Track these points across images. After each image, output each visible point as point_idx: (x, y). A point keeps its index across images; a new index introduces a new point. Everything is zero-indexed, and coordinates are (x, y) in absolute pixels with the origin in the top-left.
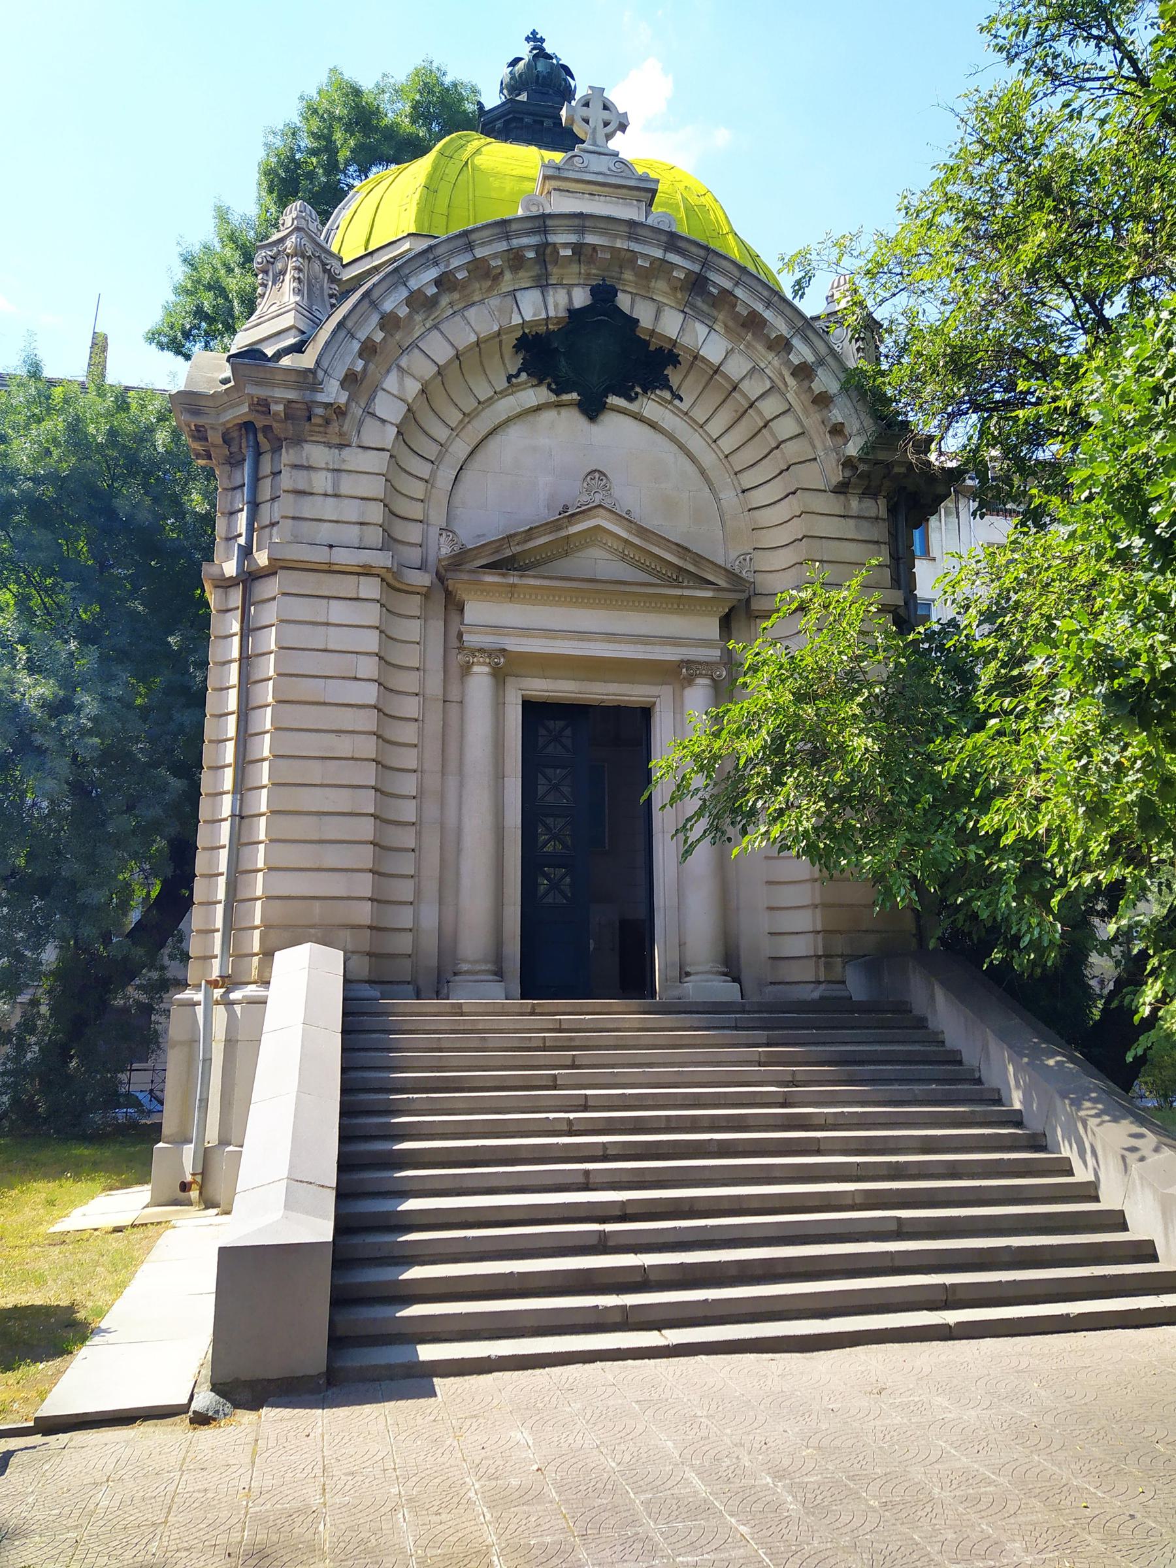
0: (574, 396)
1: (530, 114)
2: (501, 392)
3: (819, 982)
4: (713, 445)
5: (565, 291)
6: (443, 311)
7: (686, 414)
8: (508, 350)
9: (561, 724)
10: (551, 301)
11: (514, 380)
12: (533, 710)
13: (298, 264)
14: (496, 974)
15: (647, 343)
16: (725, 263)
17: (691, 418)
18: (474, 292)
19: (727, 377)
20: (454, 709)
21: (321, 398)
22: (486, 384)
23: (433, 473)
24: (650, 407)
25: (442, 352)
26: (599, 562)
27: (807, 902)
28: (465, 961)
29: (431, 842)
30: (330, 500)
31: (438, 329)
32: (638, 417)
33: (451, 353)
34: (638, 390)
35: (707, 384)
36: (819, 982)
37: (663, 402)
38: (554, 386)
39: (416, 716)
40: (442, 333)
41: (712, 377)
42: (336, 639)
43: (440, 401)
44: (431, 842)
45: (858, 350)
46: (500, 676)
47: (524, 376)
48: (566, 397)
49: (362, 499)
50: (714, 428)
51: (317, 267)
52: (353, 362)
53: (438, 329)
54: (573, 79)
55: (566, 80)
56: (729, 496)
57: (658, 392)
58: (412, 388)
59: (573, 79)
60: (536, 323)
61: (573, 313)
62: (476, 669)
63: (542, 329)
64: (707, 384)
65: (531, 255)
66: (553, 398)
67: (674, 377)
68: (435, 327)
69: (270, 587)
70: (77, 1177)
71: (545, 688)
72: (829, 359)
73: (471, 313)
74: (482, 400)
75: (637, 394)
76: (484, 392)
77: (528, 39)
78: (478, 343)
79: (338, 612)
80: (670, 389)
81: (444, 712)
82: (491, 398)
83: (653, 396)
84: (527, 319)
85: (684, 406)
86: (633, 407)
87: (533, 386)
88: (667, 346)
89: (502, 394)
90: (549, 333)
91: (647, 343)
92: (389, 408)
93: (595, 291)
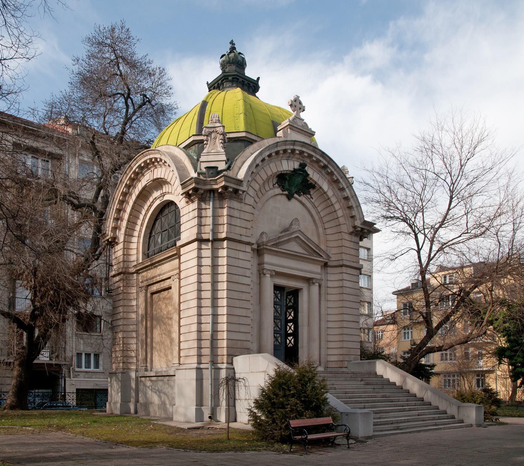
8: (275, 176)
16: (333, 164)
21: (241, 188)
24: (303, 198)
26: (295, 247)
27: (219, 275)
30: (238, 219)
32: (301, 202)
37: (307, 198)
47: (277, 185)
48: (285, 193)
56: (321, 230)
61: (295, 170)
66: (281, 192)
67: (312, 191)
79: (241, 255)
80: (310, 195)
88: (314, 183)
91: (308, 181)
93: (301, 165)
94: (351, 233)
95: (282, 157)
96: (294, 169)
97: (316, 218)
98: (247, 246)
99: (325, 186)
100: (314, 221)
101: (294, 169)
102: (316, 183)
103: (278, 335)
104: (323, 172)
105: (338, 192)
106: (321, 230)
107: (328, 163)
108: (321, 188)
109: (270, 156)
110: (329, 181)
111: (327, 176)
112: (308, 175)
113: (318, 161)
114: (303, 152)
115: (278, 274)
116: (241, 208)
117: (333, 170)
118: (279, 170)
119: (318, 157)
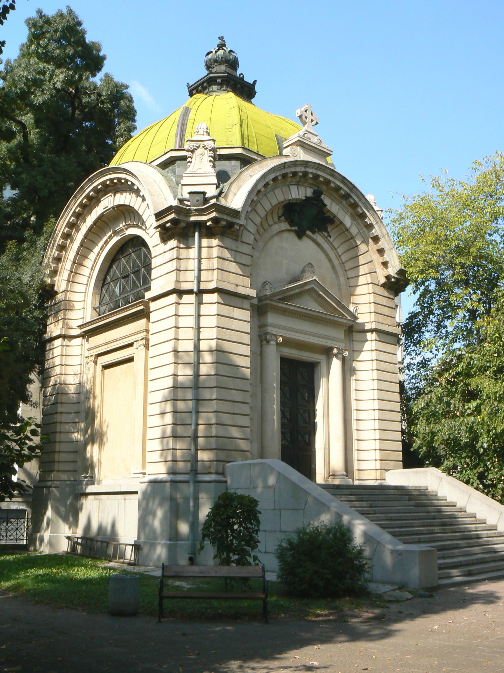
3: (377, 480)
8: (282, 206)
10: (300, 192)
11: (281, 219)
15: (325, 214)
19: (350, 233)
21: (237, 221)
24: (318, 237)
34: (316, 230)
35: (341, 234)
47: (283, 218)
48: (293, 228)
56: (342, 279)
60: (294, 199)
64: (341, 234)
65: (301, 174)
69: (206, 298)
70: (296, 649)
72: (386, 236)
77: (219, 38)
80: (328, 232)
84: (293, 198)
85: (331, 240)
88: (332, 217)
89: (275, 223)
90: (296, 204)
91: (325, 214)
93: (315, 192)
94: (383, 286)
97: (336, 263)
98: (245, 301)
99: (347, 221)
100: (333, 267)
101: (306, 197)
102: (335, 216)
104: (344, 203)
105: (365, 229)
106: (342, 279)
108: (341, 223)
111: (349, 208)
113: (337, 189)
115: (288, 343)
117: (357, 200)
119: (338, 183)
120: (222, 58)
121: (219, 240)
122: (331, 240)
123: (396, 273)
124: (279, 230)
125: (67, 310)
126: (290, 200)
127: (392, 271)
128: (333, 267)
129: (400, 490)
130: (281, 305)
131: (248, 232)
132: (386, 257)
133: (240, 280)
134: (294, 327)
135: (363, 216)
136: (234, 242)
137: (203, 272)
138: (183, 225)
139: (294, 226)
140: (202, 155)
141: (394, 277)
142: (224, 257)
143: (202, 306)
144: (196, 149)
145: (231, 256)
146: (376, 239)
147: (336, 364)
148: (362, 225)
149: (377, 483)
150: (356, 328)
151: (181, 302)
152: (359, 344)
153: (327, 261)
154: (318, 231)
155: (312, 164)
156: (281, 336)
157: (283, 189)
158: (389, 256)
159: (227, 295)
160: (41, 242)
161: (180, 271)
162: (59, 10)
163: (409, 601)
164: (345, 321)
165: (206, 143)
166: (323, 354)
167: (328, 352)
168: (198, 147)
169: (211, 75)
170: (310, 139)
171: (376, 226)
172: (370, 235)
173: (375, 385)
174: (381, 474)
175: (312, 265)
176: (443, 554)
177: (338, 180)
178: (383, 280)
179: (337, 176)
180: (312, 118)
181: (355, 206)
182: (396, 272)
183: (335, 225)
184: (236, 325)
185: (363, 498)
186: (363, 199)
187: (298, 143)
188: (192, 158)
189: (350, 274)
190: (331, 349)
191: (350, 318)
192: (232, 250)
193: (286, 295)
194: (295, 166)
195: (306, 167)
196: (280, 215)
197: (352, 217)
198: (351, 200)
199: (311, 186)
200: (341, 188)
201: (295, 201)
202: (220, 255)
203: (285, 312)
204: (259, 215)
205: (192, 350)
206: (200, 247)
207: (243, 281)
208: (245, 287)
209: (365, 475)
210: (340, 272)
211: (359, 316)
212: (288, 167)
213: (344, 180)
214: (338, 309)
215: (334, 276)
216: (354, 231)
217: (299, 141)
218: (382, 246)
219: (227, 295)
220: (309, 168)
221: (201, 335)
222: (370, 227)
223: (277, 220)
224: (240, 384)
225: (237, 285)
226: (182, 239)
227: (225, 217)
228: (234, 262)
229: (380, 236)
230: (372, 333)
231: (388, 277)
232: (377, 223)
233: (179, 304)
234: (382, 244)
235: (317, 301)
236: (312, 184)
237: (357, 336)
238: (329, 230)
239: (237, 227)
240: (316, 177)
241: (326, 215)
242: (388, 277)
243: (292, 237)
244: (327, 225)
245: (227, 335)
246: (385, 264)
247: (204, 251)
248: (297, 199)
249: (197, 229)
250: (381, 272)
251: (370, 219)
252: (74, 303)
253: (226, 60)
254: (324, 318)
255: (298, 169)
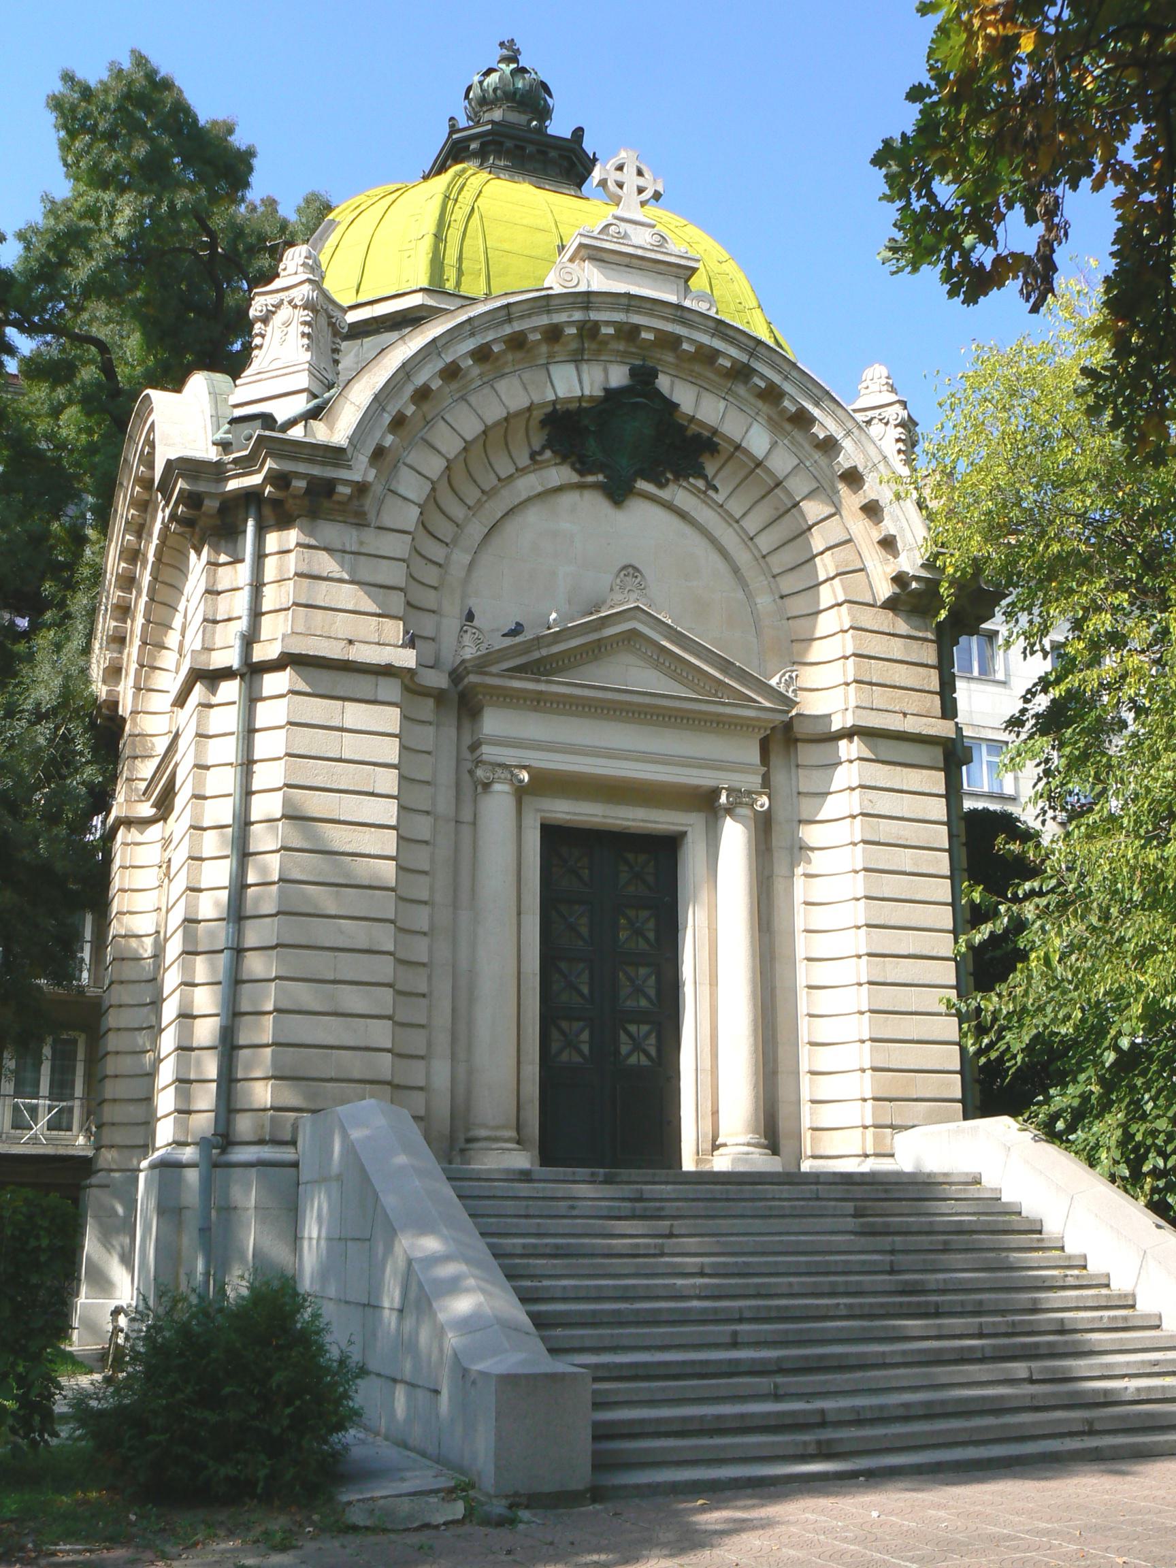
0: (601, 478)
1: (512, 138)
2: (523, 469)
3: (867, 1156)
4: (749, 543)
5: (601, 368)
6: (472, 380)
7: (721, 506)
8: (534, 423)
9: (642, 858)
10: (585, 377)
11: (539, 458)
12: (553, 835)
13: (308, 319)
14: (518, 1143)
17: (727, 512)
18: (506, 363)
19: (768, 471)
20: (466, 831)
21: (343, 474)
22: (506, 459)
23: (447, 557)
24: (679, 495)
25: (471, 428)
28: (485, 1126)
29: (443, 988)
31: (466, 401)
32: (669, 506)
33: (479, 428)
34: (670, 476)
35: (746, 478)
36: (867, 1156)
37: (696, 492)
38: (578, 466)
39: (426, 838)
40: (470, 405)
41: (753, 471)
42: (351, 746)
43: (459, 477)
44: (443, 988)
45: (899, 451)
46: (521, 792)
47: (548, 454)
48: (590, 479)
49: (381, 586)
50: (752, 524)
51: (323, 321)
52: (383, 437)
53: (466, 401)
54: (551, 96)
55: (545, 100)
56: (764, 601)
57: (691, 480)
58: (434, 467)
59: (551, 96)
60: (569, 400)
61: (611, 394)
62: (497, 787)
63: (574, 406)
64: (746, 478)
65: (573, 331)
66: (575, 478)
68: (463, 398)
69: (274, 682)
71: (566, 810)
73: (502, 386)
74: (503, 476)
75: (668, 480)
76: (505, 469)
77: (502, 44)
78: (506, 419)
79: (355, 715)
80: (705, 477)
81: (457, 833)
82: (511, 476)
83: (684, 484)
84: (561, 395)
85: (719, 498)
86: (664, 494)
87: (556, 464)
88: (706, 434)
89: (522, 471)
90: (580, 410)
92: (412, 486)
93: (634, 372)
94: (891, 604)
95: (551, 356)
96: (606, 390)
97: (743, 558)
98: (383, 681)
99: (758, 440)
100: (736, 570)
101: (606, 390)
102: (715, 432)
103: (645, 1028)
104: (741, 390)
105: (817, 455)
106: (764, 601)
107: (751, 355)
108: (738, 447)
109: (482, 355)
110: (770, 419)
111: (760, 404)
112: (676, 406)
113: (708, 356)
114: (637, 329)
115: (546, 784)
116: (361, 543)
117: (777, 379)
118: (537, 399)
119: (705, 339)
120: (495, 90)
121: (301, 529)
122: (719, 498)
123: (923, 566)
124: (540, 489)
125: (136, 758)
126: (554, 403)
127: (910, 562)
128: (736, 570)
129: (882, 1184)
130: (516, 684)
131: (400, 502)
132: (889, 526)
133: (368, 627)
134: (597, 744)
135: (803, 420)
136: (354, 532)
137: (265, 620)
138: (211, 505)
139: (591, 473)
140: (287, 324)
141: (917, 578)
142: (315, 573)
143: (260, 706)
144: (274, 313)
145: (342, 566)
146: (853, 478)
147: (734, 837)
148: (807, 446)
149: (867, 1166)
150: (800, 729)
151: (214, 700)
152: (816, 774)
153: (715, 557)
154: (677, 479)
155: (609, 300)
156: (524, 767)
157: (526, 376)
158: (896, 520)
159: (319, 670)
160: (79, 602)
161: (215, 622)
162: (112, 63)
163: (432, 1532)
164: (751, 713)
165: (293, 293)
166: (700, 810)
167: (707, 803)
168: (278, 306)
169: (454, 136)
170: (626, 236)
171: (847, 444)
172: (836, 468)
173: (858, 885)
174: (877, 1140)
175: (636, 569)
176: (776, 1386)
177: (705, 332)
178: (885, 590)
179: (697, 319)
180: (641, 182)
181: (772, 395)
182: (920, 562)
183: (723, 457)
184: (351, 746)
185: (662, 1209)
186: (794, 373)
187: (583, 252)
188: (263, 336)
189: (788, 584)
190: (716, 792)
191: (768, 705)
192: (344, 552)
193: (536, 655)
194: (549, 312)
195: (587, 308)
196: (537, 448)
197: (774, 425)
198: (757, 380)
199: (622, 358)
200: (717, 353)
201: (575, 405)
202: (304, 569)
203: (538, 703)
204: (439, 452)
205: (230, 822)
206: (260, 556)
207: (379, 631)
208: (383, 643)
209: (832, 1144)
210: (757, 581)
211: (801, 697)
212: (521, 317)
213: (722, 328)
214: (727, 680)
215: (740, 595)
216: (781, 463)
217: (581, 246)
218: (873, 496)
219: (319, 670)
220: (598, 309)
221: (254, 781)
222: (829, 446)
223: (528, 462)
224: (355, 902)
225: (351, 642)
226: (223, 543)
227: (302, 468)
228: (352, 582)
229: (861, 469)
230: (851, 741)
231: (900, 579)
232: (849, 433)
233: (211, 706)
234: (873, 489)
235: (657, 666)
236: (625, 354)
237: (808, 754)
238: (710, 470)
239: (344, 490)
240: (630, 333)
241: (689, 433)
242: (900, 579)
243: (593, 505)
244: (701, 460)
245: (319, 773)
246: (888, 543)
247: (271, 565)
248: (580, 399)
249: (253, 511)
250: (880, 569)
251: (826, 424)
252: (154, 739)
253: (505, 93)
254: (730, 716)
255: (561, 318)
